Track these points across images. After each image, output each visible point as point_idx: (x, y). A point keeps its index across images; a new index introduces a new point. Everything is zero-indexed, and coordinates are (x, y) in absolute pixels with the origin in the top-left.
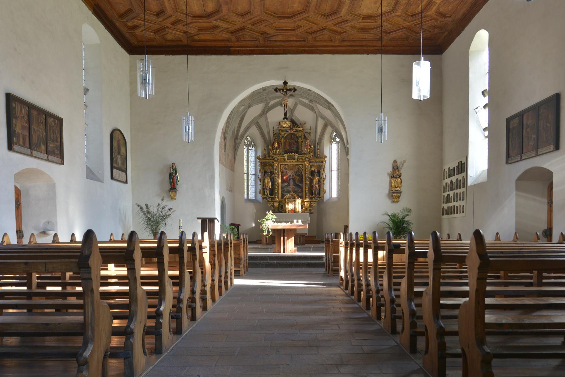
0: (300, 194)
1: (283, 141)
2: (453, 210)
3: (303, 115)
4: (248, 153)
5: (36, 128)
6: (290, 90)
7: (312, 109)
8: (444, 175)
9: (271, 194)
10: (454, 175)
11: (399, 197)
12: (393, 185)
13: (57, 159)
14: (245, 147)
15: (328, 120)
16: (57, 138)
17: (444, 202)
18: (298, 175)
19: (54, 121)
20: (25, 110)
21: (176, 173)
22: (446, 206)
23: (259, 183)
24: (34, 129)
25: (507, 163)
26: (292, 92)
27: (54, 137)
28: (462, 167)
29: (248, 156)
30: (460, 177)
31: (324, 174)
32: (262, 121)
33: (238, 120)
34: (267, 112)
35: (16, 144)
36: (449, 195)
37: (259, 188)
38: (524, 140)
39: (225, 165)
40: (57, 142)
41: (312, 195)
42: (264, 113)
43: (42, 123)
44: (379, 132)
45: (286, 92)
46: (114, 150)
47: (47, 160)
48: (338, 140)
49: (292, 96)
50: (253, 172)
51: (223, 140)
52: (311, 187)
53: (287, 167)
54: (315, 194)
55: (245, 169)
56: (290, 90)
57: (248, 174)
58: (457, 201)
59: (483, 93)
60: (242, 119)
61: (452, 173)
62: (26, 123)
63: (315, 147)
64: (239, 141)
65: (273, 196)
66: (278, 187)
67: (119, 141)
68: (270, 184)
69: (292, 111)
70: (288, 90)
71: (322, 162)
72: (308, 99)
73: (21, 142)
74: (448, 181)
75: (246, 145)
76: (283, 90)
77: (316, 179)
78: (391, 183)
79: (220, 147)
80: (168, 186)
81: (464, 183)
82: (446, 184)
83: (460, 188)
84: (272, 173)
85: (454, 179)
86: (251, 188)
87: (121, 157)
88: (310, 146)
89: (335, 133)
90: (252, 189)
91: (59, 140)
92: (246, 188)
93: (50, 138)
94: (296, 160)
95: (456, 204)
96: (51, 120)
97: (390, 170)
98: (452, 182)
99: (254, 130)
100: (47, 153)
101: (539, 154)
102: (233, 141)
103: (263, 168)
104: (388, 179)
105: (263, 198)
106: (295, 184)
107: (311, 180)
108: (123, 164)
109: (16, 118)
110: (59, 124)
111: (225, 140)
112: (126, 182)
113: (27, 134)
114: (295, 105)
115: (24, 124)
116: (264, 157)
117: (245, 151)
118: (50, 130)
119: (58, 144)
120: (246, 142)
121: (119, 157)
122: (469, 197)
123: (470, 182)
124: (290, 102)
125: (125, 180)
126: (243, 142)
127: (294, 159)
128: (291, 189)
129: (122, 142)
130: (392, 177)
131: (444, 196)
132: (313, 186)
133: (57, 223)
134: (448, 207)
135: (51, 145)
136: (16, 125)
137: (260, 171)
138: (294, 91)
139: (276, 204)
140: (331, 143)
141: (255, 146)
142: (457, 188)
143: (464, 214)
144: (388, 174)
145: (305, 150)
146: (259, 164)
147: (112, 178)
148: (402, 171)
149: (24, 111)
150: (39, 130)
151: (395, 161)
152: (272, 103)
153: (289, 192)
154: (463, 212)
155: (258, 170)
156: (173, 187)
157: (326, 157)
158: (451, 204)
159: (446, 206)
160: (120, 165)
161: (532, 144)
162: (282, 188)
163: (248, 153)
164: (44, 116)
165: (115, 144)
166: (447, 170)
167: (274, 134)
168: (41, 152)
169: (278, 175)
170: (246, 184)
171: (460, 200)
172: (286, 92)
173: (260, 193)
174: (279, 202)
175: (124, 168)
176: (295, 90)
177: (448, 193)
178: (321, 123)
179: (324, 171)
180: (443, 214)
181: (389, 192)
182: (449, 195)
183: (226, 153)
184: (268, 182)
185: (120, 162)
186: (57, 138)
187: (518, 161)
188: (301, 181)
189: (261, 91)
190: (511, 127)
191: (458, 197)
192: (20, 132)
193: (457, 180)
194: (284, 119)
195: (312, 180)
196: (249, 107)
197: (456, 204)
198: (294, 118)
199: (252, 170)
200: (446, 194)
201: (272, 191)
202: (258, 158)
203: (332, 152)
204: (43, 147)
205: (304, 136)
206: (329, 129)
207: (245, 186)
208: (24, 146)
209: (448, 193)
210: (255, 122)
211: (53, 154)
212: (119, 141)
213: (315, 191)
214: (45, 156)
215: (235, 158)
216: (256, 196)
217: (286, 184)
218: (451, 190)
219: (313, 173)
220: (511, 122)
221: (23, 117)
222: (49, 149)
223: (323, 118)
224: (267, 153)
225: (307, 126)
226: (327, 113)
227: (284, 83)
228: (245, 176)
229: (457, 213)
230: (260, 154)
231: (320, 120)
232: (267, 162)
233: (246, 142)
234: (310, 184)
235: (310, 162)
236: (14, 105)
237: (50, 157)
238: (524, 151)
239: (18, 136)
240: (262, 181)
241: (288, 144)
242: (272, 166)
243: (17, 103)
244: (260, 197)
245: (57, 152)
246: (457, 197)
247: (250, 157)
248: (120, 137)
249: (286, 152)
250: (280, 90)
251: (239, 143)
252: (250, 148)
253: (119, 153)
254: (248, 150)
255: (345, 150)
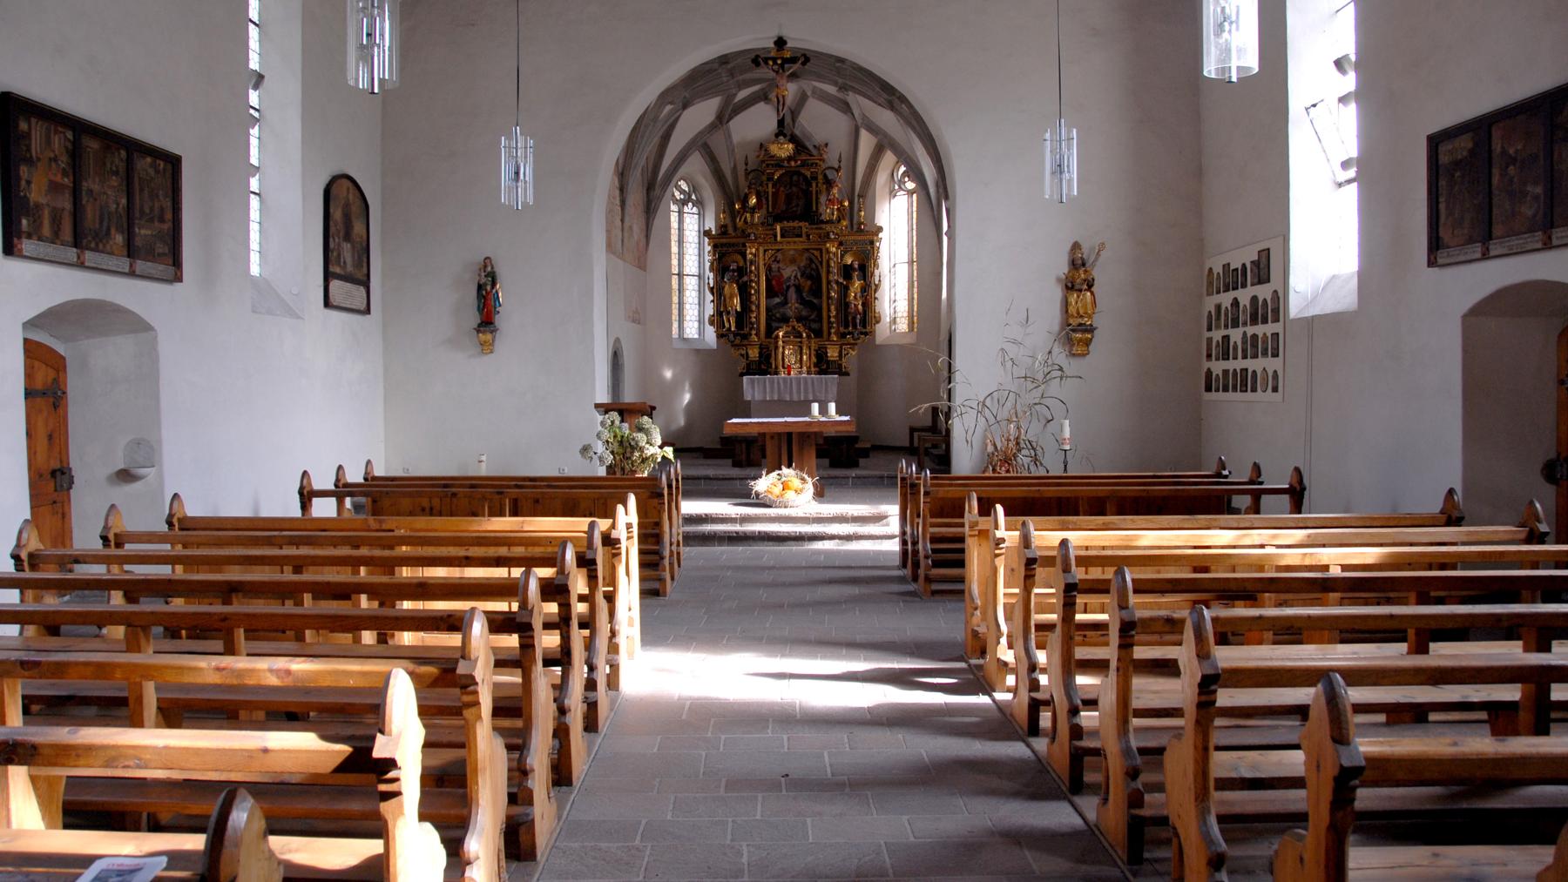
0: (814, 326)
1: (770, 190)
2: (1244, 382)
3: (823, 123)
4: (681, 221)
5: (96, 187)
6: (793, 60)
7: (846, 108)
8: (1210, 284)
9: (739, 325)
10: (1244, 286)
11: (1088, 343)
12: (1072, 310)
13: (161, 267)
14: (674, 208)
15: (886, 135)
16: (162, 209)
17: (1209, 356)
18: (810, 277)
19: (154, 165)
20: (60, 141)
21: (494, 284)
22: (1218, 367)
23: (709, 297)
24: (90, 191)
25: (1431, 263)
26: (795, 67)
27: (152, 209)
28: (1266, 266)
29: (681, 229)
30: (1263, 292)
31: (877, 272)
32: (717, 142)
33: (656, 140)
34: (731, 118)
35: (29, 236)
36: (1226, 338)
37: (710, 309)
38: (1495, 200)
39: (621, 257)
40: (162, 220)
41: (846, 327)
42: (722, 119)
43: (116, 173)
44: (1053, 173)
45: (782, 66)
46: (332, 229)
47: (132, 274)
48: (910, 185)
49: (794, 76)
50: (695, 271)
51: (617, 192)
52: (844, 304)
53: (780, 256)
54: (855, 326)
55: (675, 262)
56: (793, 60)
57: (680, 275)
58: (1255, 356)
59: (1339, 64)
60: (666, 138)
61: (1233, 279)
62: (65, 173)
63: (851, 203)
64: (657, 191)
65: (746, 330)
66: (758, 307)
67: (347, 206)
68: (736, 301)
69: (795, 114)
70: (786, 61)
71: (872, 243)
72: (835, 84)
73: (46, 230)
74: (1226, 299)
75: (676, 201)
76: (774, 60)
77: (857, 284)
78: (1066, 304)
79: (609, 212)
80: (474, 319)
81: (1276, 311)
82: (1218, 307)
83: (1265, 321)
84: (741, 271)
85: (1244, 296)
86: (693, 316)
87: (353, 248)
88: (841, 203)
89: (903, 169)
90: (691, 312)
91: (169, 216)
92: (675, 312)
93: (142, 212)
94: (803, 239)
95: (1252, 365)
96: (144, 164)
97: (1063, 268)
98: (1236, 303)
99: (696, 165)
100: (131, 252)
101: (1555, 242)
102: (643, 188)
103: (720, 259)
104: (1058, 293)
105: (720, 336)
106: (802, 301)
107: (845, 290)
108: (358, 265)
109: (30, 162)
110: (169, 174)
111: (622, 190)
112: (368, 311)
113: (68, 206)
114: (802, 99)
115: (58, 178)
116: (723, 230)
117: (674, 218)
118: (142, 190)
119: (167, 226)
120: (677, 194)
121: (347, 246)
122: (1293, 349)
123: (1297, 306)
124: (791, 90)
125: (363, 307)
126: (668, 194)
127: (800, 236)
128: (790, 313)
129: (356, 208)
130: (1070, 286)
131: (1210, 340)
132: (847, 305)
133: (160, 442)
134: (1226, 372)
135: (143, 232)
136: (29, 183)
137: (711, 269)
138: (804, 64)
139: (754, 353)
140: (892, 194)
141: (699, 204)
142: (1254, 321)
143: (1277, 396)
144: (1059, 280)
145: (828, 212)
146: (708, 248)
147: (327, 303)
148: (1096, 273)
149: (57, 141)
150: (106, 192)
151: (1076, 246)
152: (743, 94)
153: (785, 320)
154: (1275, 389)
155: (708, 265)
156: (487, 321)
157: (880, 229)
158: (1231, 365)
159: (1218, 367)
160: (350, 268)
161: (1530, 213)
162: (768, 310)
163: (681, 221)
164: (123, 153)
165: (337, 214)
166: (1218, 269)
167: (747, 173)
168: (111, 253)
169: (758, 276)
170: (675, 299)
171: (1265, 354)
172: (782, 66)
173: (711, 323)
174: (761, 348)
175: (360, 276)
176: (807, 60)
177: (1223, 332)
178: (867, 142)
179: (876, 265)
180: (1208, 389)
181: (1062, 329)
182: (1226, 338)
183: (627, 224)
184: (731, 297)
185: (349, 261)
186: (162, 209)
187: (1470, 261)
188: (817, 292)
189: (716, 65)
190: (1444, 159)
191: (1253, 347)
192: (43, 200)
193: (1254, 299)
194: (777, 135)
195: (847, 288)
196: (685, 107)
197: (1252, 365)
198: (797, 132)
199: (691, 265)
200: (1217, 335)
201: (742, 318)
202: (707, 233)
203: (895, 218)
204: (119, 239)
205: (825, 176)
206: (889, 158)
207: (675, 307)
208: (55, 238)
209: (1223, 332)
210: (702, 144)
211: (150, 255)
212: (347, 206)
213: (854, 318)
214: (124, 264)
215: (647, 237)
216: (701, 331)
217: (777, 300)
218: (1235, 324)
219: (847, 271)
220: (1443, 148)
221: (55, 159)
222: (138, 242)
223: (873, 129)
224: (728, 221)
225: (831, 158)
226: (886, 119)
227: (776, 43)
228: (675, 280)
229: (1254, 390)
230: (710, 224)
231: (865, 136)
232: (730, 245)
233: (677, 194)
234: (839, 299)
235: (841, 244)
236: (23, 126)
237: (140, 266)
238: (1497, 230)
239: (34, 212)
240: (718, 291)
241: (782, 198)
242: (744, 255)
243: (33, 121)
244: (711, 333)
245: (161, 248)
246: (1254, 346)
247: (687, 233)
248: (352, 196)
249: (778, 218)
250: (766, 60)
251: (660, 199)
252: (686, 209)
253: (348, 237)
254: (681, 213)
255: (935, 203)
